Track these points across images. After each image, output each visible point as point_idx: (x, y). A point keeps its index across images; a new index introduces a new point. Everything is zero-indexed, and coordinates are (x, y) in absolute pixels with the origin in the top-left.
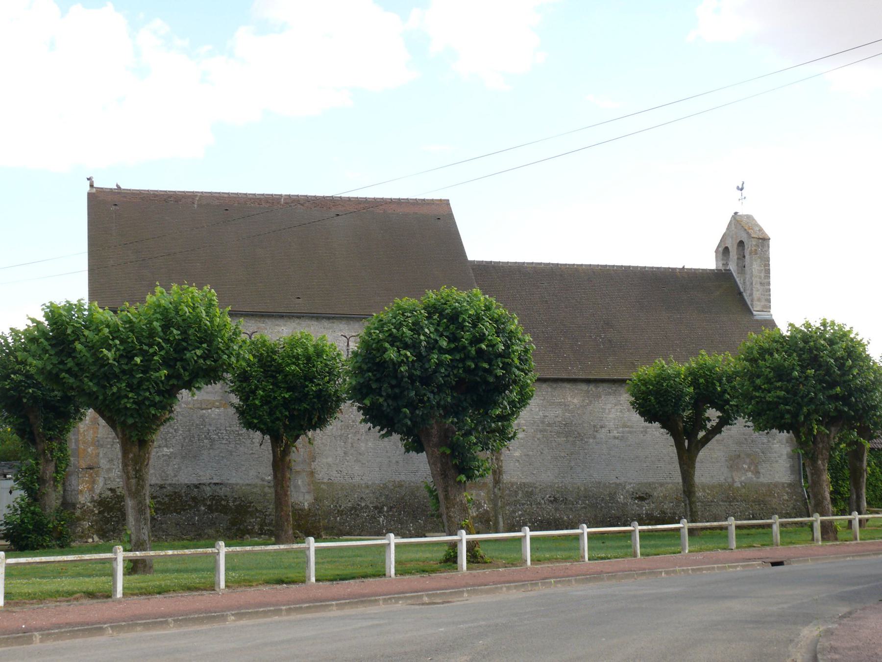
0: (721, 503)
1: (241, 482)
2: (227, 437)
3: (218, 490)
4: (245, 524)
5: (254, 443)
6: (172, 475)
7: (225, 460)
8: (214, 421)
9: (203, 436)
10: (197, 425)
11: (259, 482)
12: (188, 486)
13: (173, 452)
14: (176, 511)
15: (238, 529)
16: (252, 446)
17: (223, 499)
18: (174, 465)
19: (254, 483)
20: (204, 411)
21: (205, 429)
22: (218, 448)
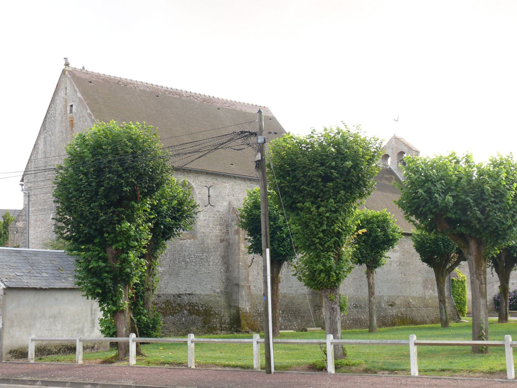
0: (423, 308)
1: (202, 293)
2: (195, 261)
3: (191, 299)
4: (212, 323)
5: (210, 265)
6: (164, 287)
7: (194, 277)
8: (188, 249)
9: (181, 259)
10: (178, 251)
11: (211, 292)
12: (174, 296)
13: (164, 270)
14: (170, 314)
15: (209, 327)
16: (209, 267)
17: (196, 306)
18: (165, 280)
19: (210, 294)
20: (182, 241)
21: (182, 254)
22: (190, 268)
